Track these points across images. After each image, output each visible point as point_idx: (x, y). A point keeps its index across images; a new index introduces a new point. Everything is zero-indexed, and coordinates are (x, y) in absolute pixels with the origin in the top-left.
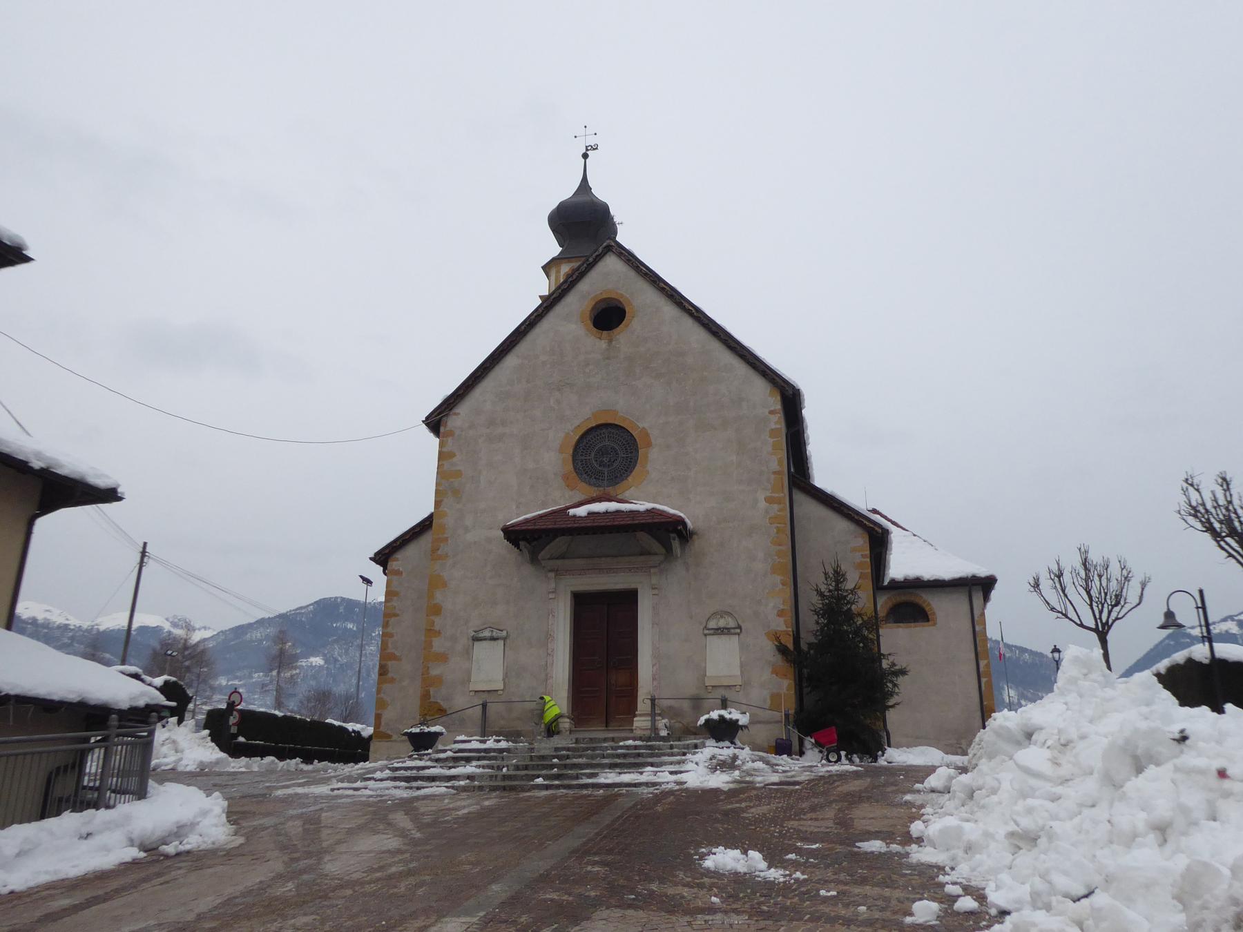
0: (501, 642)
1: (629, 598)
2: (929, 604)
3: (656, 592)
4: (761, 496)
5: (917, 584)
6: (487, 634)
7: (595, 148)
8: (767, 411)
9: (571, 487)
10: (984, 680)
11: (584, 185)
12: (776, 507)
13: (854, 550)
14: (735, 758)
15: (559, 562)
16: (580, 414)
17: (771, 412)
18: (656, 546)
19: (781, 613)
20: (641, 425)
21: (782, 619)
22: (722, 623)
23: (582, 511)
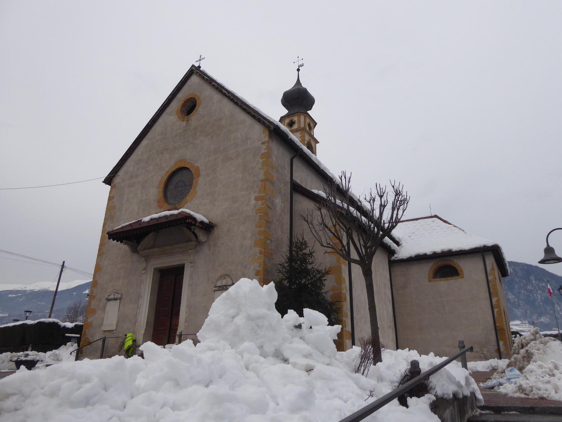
0: (118, 301)
2: (459, 266)
3: (192, 265)
4: (253, 197)
6: (112, 297)
7: (302, 65)
8: (260, 143)
12: (260, 202)
14: (527, 351)
16: (169, 164)
17: (263, 143)
18: (189, 233)
20: (196, 165)
23: (146, 219)
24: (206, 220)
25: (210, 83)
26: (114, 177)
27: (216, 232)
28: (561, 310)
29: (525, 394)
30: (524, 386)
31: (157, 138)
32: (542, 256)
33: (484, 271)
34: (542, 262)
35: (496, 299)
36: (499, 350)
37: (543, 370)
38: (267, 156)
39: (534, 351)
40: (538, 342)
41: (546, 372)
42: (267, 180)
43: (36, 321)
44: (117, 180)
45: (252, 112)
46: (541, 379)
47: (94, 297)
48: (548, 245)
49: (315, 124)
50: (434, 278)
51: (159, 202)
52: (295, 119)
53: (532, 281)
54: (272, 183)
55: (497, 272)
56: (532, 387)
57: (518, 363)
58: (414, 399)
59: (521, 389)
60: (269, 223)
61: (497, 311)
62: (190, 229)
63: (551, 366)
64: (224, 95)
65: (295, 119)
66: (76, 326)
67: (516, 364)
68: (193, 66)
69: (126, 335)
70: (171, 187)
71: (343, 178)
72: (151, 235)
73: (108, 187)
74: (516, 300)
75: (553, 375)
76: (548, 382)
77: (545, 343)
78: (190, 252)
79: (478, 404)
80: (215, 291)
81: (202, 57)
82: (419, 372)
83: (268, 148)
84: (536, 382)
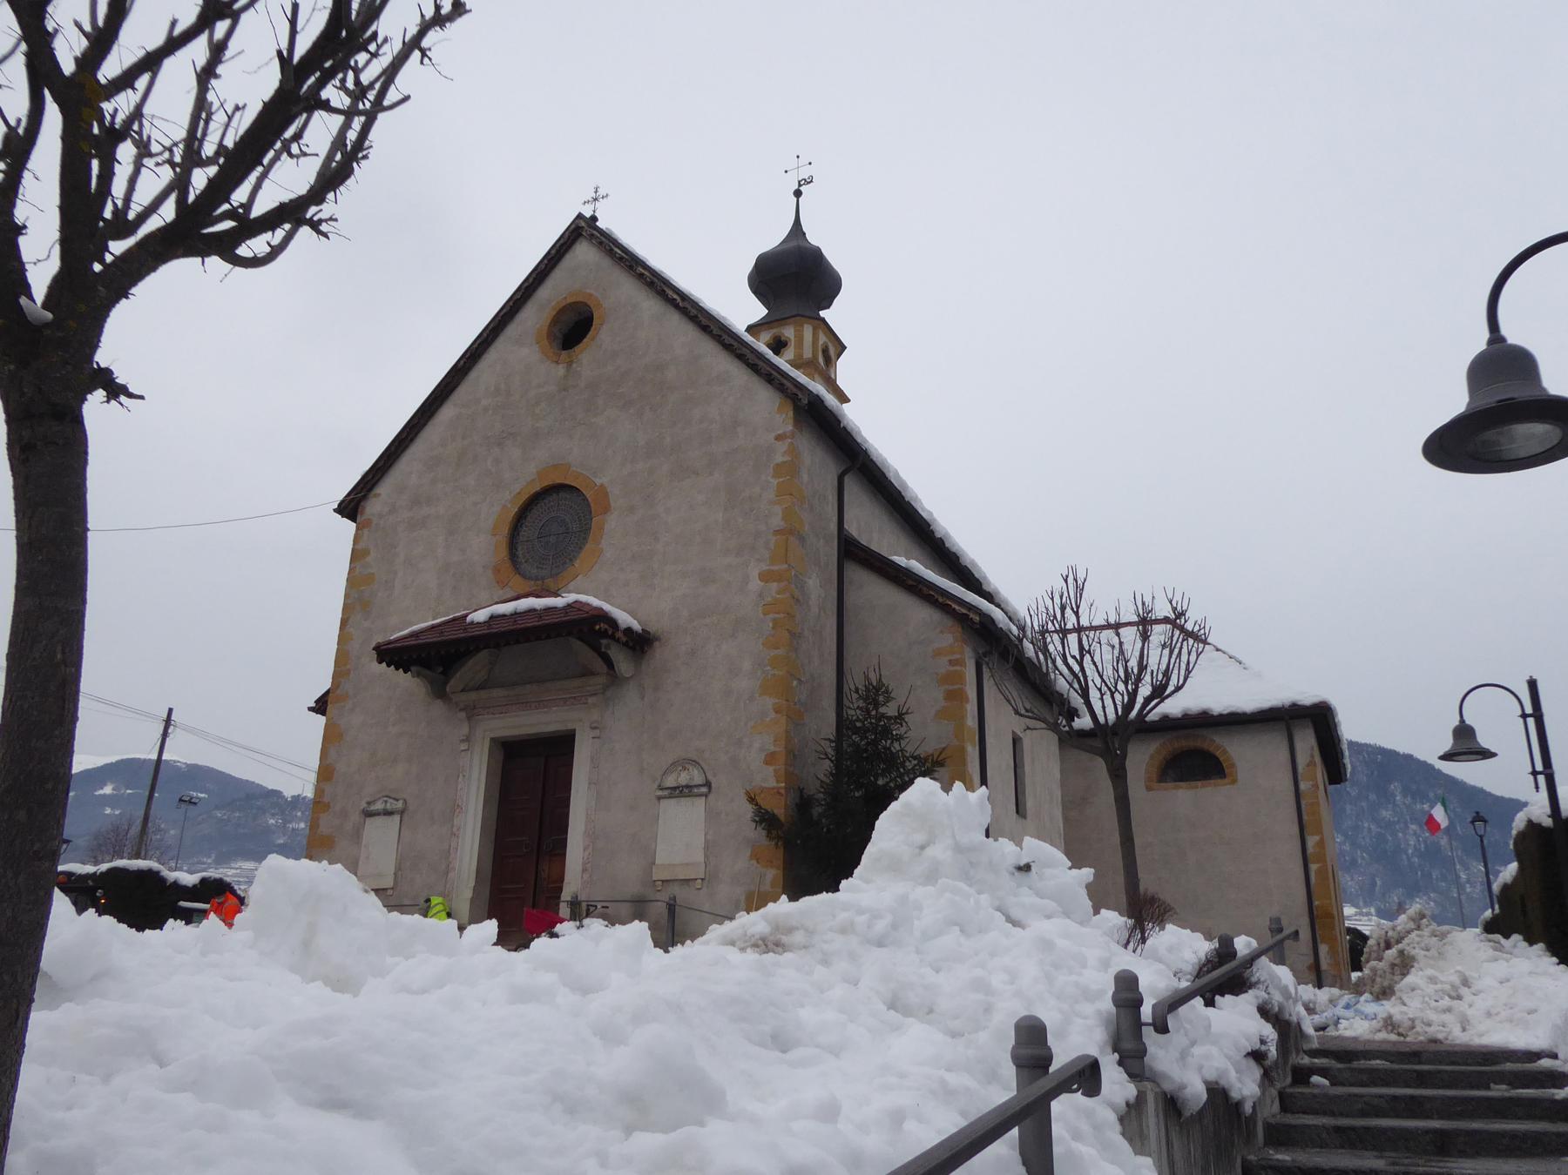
0: (397, 818)
1: (560, 747)
2: (1225, 752)
3: (597, 733)
5: (1203, 721)
6: (379, 806)
7: (809, 181)
9: (502, 584)
10: (1313, 867)
11: (797, 229)
13: (938, 653)
14: (1401, 952)
15: (473, 695)
16: (522, 474)
17: (779, 438)
19: (770, 759)
20: (598, 481)
21: (771, 768)
22: (683, 779)
23: (480, 616)
24: (636, 626)
25: (631, 267)
26: (365, 497)
27: (659, 653)
28: (1468, 881)
29: (1399, 1034)
30: (1397, 1017)
31: (484, 402)
32: (1447, 743)
33: (1289, 767)
34: (1446, 757)
35: (1317, 838)
36: (1316, 967)
37: (1439, 986)
38: (789, 470)
39: (1418, 952)
40: (1426, 932)
41: (1443, 991)
42: (790, 532)
43: (104, 867)
44: (373, 507)
45: (749, 355)
46: (1433, 1004)
47: (328, 806)
48: (1462, 721)
49: (842, 348)
50: (1160, 781)
51: (497, 570)
52: (789, 332)
53: (1394, 795)
54: (802, 539)
55: (1320, 772)
56: (1413, 1020)
57: (1378, 980)
58: (1228, 997)
59: (1390, 1024)
60: (795, 636)
61: (1318, 872)
62: (596, 649)
63: (1456, 979)
64: (672, 303)
65: (789, 332)
66: (203, 880)
67: (1374, 981)
68: (580, 216)
69: (428, 901)
70: (525, 533)
71: (1071, 580)
72: (483, 656)
73: (350, 527)
74: (1347, 847)
75: (1459, 998)
76: (1449, 1010)
77: (1443, 936)
78: (590, 700)
79: (1306, 1047)
80: (659, 798)
81: (601, 192)
82: (1235, 954)
83: (793, 451)
84: (1422, 1010)
